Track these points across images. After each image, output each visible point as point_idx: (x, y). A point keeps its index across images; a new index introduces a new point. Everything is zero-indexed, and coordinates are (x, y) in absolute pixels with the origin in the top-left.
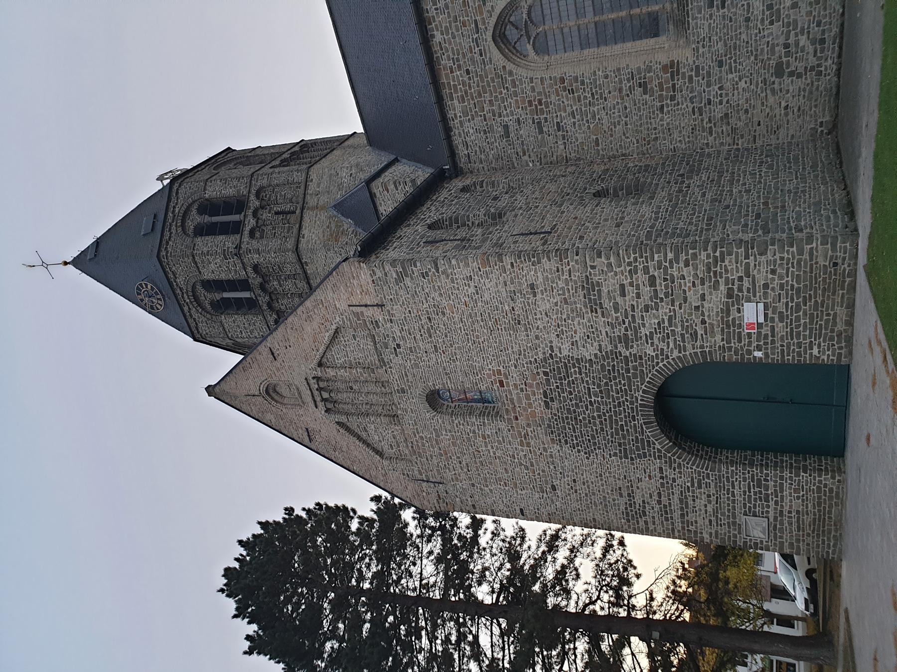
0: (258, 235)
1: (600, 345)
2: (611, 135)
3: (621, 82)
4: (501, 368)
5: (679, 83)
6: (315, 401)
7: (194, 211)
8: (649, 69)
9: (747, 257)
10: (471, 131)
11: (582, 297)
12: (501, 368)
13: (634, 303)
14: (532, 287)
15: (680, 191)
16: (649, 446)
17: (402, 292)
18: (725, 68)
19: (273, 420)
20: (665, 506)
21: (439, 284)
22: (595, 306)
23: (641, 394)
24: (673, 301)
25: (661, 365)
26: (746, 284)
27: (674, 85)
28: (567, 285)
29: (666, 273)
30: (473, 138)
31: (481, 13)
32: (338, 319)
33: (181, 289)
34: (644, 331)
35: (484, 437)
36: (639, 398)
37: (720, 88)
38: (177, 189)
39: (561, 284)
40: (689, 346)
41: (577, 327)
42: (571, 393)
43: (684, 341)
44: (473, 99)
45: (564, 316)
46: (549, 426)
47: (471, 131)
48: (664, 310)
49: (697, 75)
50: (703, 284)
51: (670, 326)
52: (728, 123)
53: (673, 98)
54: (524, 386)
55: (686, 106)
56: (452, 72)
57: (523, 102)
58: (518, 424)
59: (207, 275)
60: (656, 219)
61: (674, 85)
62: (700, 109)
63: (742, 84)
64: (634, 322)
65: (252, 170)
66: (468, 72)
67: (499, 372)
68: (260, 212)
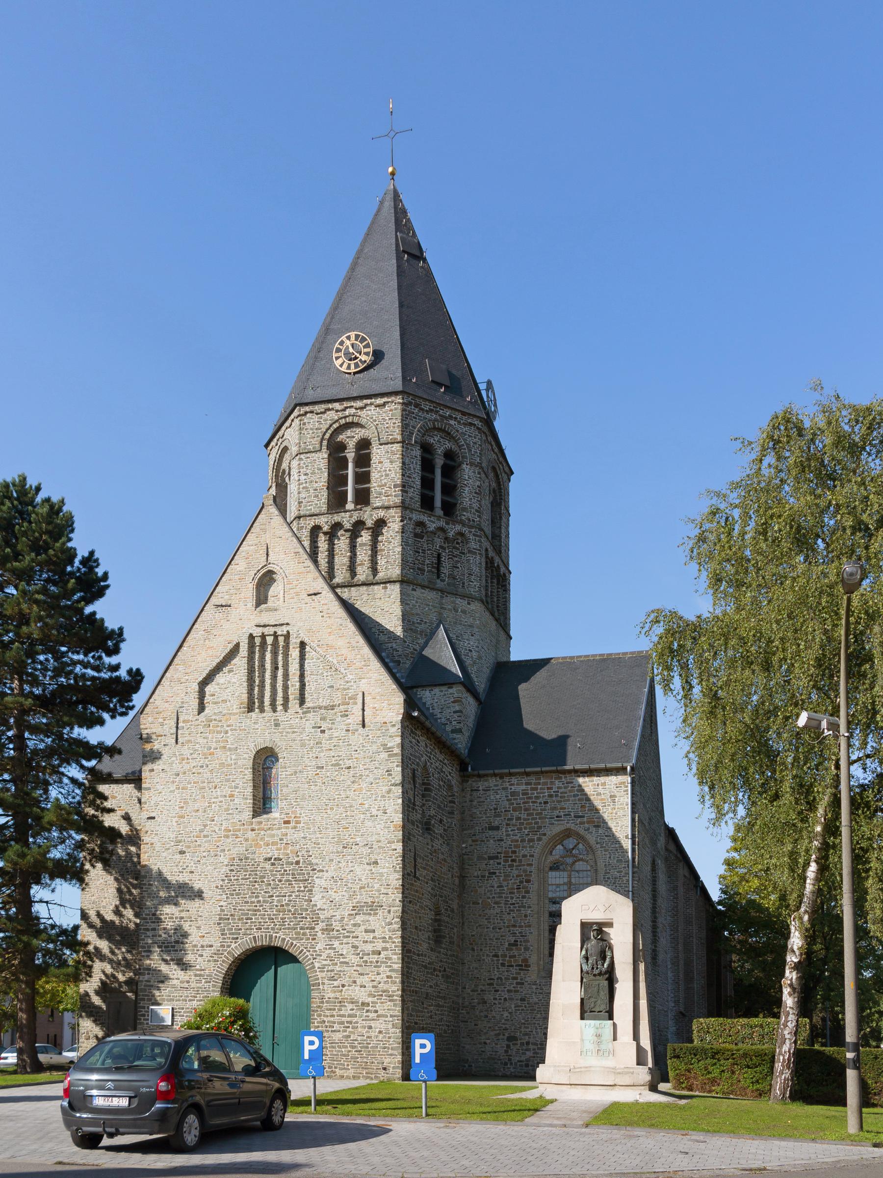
0: (418, 530)
1: (324, 910)
2: (480, 915)
3: (521, 927)
4: (302, 825)
5: (514, 970)
6: (265, 626)
7: (448, 445)
8: (526, 949)
9: (391, 1016)
10: (498, 797)
11: (365, 900)
12: (302, 825)
13: (359, 939)
14: (376, 863)
15: (435, 970)
16: (233, 939)
17: (375, 747)
18: (519, 1003)
19: (238, 568)
20: (174, 947)
21: (381, 784)
22: (357, 909)
23: (283, 938)
24: (361, 966)
25: (308, 953)
26: (372, 1015)
27: (512, 966)
28: (376, 891)
29: (382, 962)
30: (492, 797)
31: (588, 822)
32: (351, 677)
33: (361, 408)
34: (336, 944)
35: (232, 796)
36: (278, 935)
37: (505, 999)
38: (475, 425)
39: (376, 886)
40: (324, 975)
41: (340, 894)
42: (280, 881)
43: (328, 971)
44: (524, 803)
45: (350, 885)
46: (247, 858)
47: (498, 797)
48: (355, 960)
49: (517, 983)
50: (373, 987)
51: (341, 963)
52: (479, 1003)
53: (503, 965)
54: (285, 842)
55: (496, 974)
56: (548, 788)
57: (516, 846)
58: (247, 830)
59: (378, 453)
60: (418, 955)
61: (512, 966)
62: (492, 984)
63: (506, 1014)
64: (344, 937)
65: (486, 529)
66: (546, 803)
67: (298, 822)
68: (442, 535)
